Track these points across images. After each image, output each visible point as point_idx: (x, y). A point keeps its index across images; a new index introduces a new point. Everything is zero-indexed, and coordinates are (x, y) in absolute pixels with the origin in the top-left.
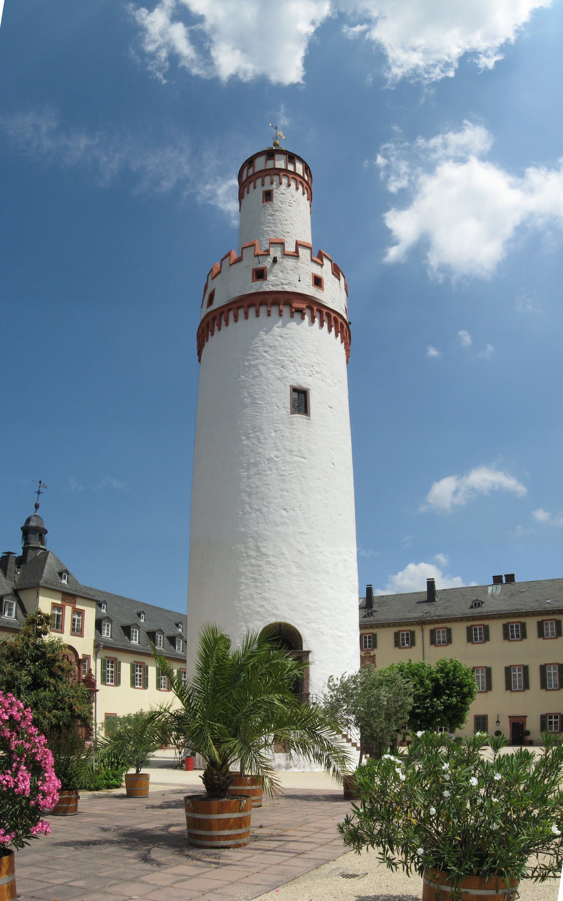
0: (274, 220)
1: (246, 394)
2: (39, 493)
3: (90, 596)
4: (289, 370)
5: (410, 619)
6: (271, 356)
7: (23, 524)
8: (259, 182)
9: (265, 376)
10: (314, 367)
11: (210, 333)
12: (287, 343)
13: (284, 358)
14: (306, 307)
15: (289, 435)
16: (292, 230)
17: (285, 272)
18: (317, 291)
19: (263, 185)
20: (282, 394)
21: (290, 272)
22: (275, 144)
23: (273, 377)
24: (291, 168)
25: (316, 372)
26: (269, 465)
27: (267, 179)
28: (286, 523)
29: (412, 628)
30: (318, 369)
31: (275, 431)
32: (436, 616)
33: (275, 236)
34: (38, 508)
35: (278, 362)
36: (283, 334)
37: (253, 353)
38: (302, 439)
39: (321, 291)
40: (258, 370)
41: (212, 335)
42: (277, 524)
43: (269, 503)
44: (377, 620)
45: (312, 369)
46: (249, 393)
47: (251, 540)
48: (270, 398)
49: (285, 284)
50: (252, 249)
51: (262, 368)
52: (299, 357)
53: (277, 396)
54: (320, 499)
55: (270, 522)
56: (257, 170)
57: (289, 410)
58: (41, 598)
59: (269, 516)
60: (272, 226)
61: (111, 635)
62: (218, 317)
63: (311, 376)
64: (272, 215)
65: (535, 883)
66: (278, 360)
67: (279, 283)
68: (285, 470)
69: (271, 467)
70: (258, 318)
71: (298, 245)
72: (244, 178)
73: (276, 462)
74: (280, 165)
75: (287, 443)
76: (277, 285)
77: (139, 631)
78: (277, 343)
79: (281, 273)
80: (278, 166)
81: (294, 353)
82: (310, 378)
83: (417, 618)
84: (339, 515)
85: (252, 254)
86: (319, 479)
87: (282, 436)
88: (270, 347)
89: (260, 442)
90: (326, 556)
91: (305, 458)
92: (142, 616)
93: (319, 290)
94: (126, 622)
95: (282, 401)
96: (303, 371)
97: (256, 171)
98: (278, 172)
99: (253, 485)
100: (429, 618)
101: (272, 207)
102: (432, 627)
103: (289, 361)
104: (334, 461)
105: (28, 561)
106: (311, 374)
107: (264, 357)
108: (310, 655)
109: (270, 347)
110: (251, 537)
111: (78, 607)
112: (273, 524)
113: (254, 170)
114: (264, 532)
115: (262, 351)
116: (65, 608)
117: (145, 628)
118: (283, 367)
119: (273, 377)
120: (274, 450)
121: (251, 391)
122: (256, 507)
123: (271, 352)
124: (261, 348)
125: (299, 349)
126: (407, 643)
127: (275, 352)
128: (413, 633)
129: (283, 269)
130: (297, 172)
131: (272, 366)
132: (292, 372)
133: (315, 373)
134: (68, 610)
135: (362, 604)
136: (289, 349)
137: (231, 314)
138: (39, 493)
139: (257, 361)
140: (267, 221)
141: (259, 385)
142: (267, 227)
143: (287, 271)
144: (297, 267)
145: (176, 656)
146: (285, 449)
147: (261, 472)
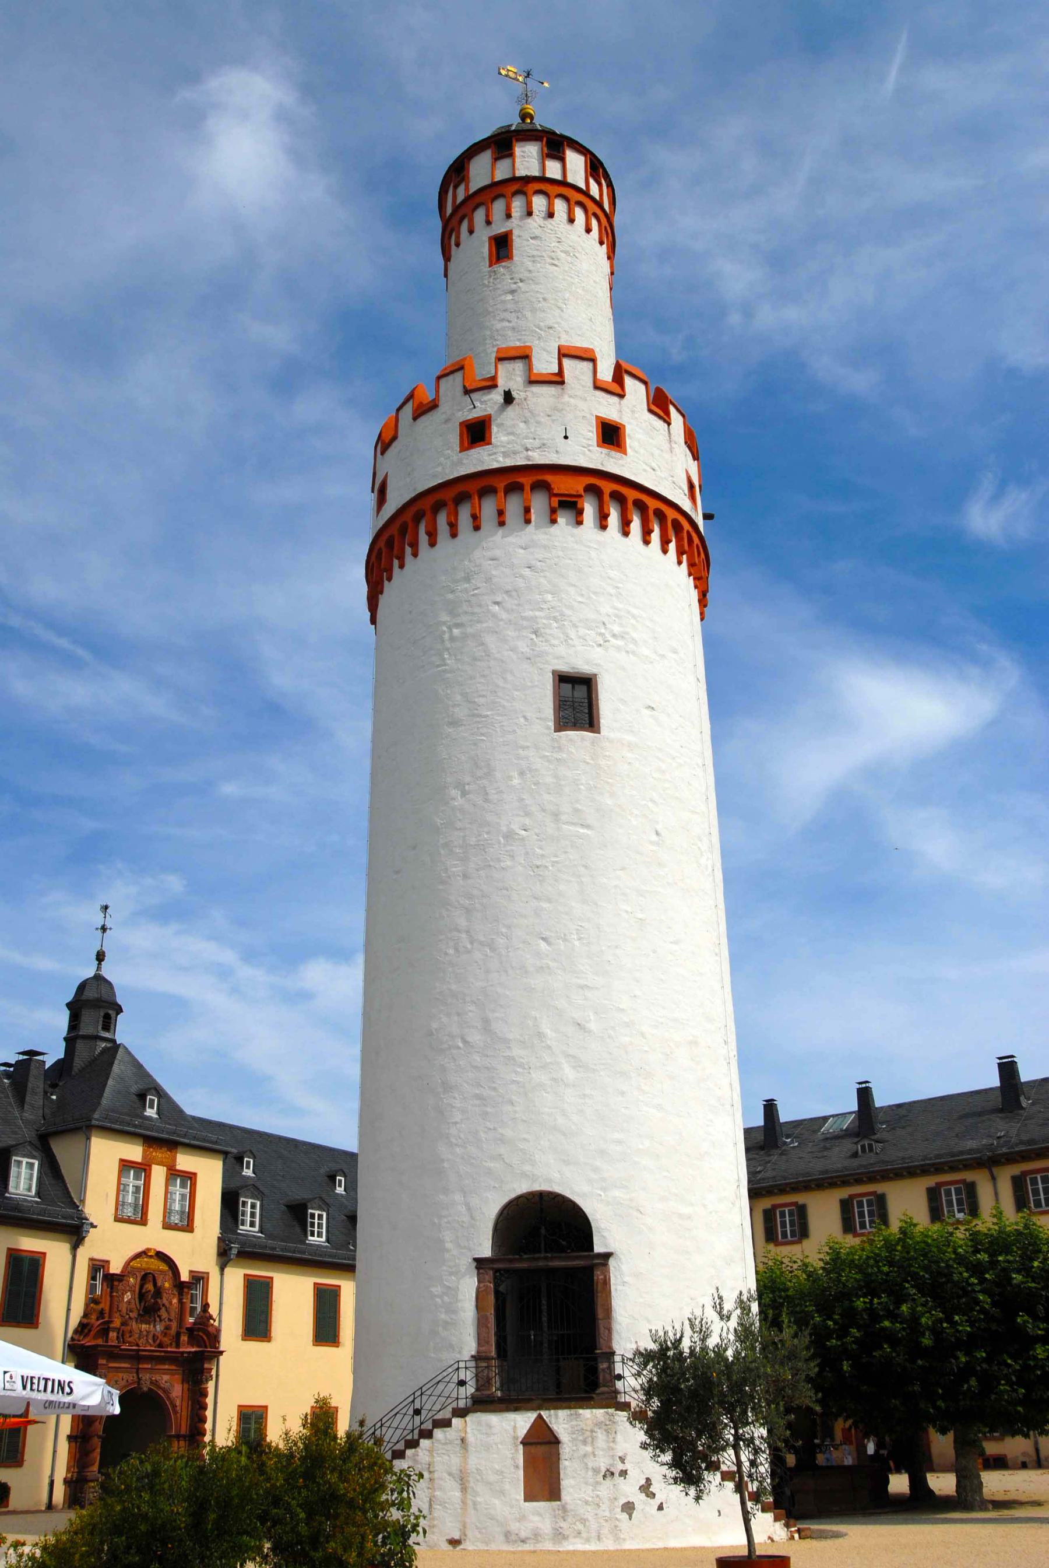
0: (516, 303)
1: (459, 697)
2: (104, 929)
3: (198, 1140)
4: (549, 638)
5: (962, 1153)
6: (507, 611)
7: (70, 997)
8: (479, 215)
9: (497, 656)
10: (608, 626)
11: (396, 562)
12: (542, 580)
13: (537, 613)
14: (585, 491)
15: (549, 780)
16: (559, 320)
17: (532, 421)
18: (608, 455)
19: (488, 223)
20: (537, 690)
21: (543, 419)
22: (524, 116)
23: (515, 657)
24: (553, 169)
25: (614, 636)
26: (509, 848)
27: (498, 206)
28: (548, 967)
29: (969, 1176)
30: (616, 629)
31: (522, 774)
32: (1022, 1142)
33: (519, 340)
34: (103, 960)
35: (525, 623)
36: (533, 562)
37: (470, 610)
38: (582, 787)
39: (619, 455)
40: (483, 644)
41: (402, 566)
42: (526, 972)
43: (509, 927)
44: (883, 1162)
45: (603, 631)
46: (464, 695)
47: (472, 1008)
48: (508, 701)
49: (533, 450)
50: (458, 376)
51: (490, 640)
52: (571, 608)
53: (523, 697)
54: (627, 912)
55: (512, 968)
56: (474, 187)
57: (551, 724)
58: (178, 1155)
59: (511, 954)
60: (512, 317)
61: (261, 1226)
62: (410, 525)
63: (600, 645)
64: (512, 292)
65: (427, 1539)
66: (524, 618)
67: (518, 448)
68: (543, 856)
69: (513, 850)
70: (478, 533)
71: (563, 354)
72: (449, 210)
73: (523, 839)
74: (528, 168)
75: (546, 797)
76: (515, 453)
77: (328, 1215)
78: (521, 584)
79: (522, 425)
80: (521, 172)
81: (560, 600)
82: (599, 649)
83: (978, 1151)
84: (676, 943)
85: (459, 390)
86: (623, 869)
87: (535, 784)
88: (507, 592)
89: (486, 800)
90: (643, 1035)
91: (588, 827)
92: (340, 1181)
93: (613, 453)
94: (298, 1194)
95: (534, 706)
96: (580, 637)
97: (473, 189)
98: (523, 185)
99: (475, 892)
100: (1005, 1150)
101: (511, 273)
102: (1016, 1169)
103: (548, 618)
104: (659, 827)
105: (75, 1070)
106: (602, 642)
107: (494, 616)
108: (612, 1262)
109: (507, 592)
110: (473, 1002)
111: (180, 1166)
112: (518, 972)
113: (467, 189)
114: (499, 990)
115: (489, 603)
116: (150, 1170)
117: (346, 1207)
118: (535, 632)
119: (515, 657)
120: (518, 815)
121: (468, 691)
122: (482, 938)
123: (510, 603)
124: (486, 597)
125: (572, 590)
126: (959, 1211)
127: (516, 602)
128: (971, 1189)
129: (528, 414)
130: (570, 180)
131: (511, 633)
132: (556, 642)
133: (610, 639)
134: (158, 1173)
135: (852, 1126)
136: (548, 592)
137: (442, 519)
138: (104, 929)
139: (479, 626)
140: (498, 306)
141: (484, 676)
142: (502, 320)
143: (537, 418)
144: (560, 406)
145: (294, 1252)
146: (544, 810)
147: (492, 863)
